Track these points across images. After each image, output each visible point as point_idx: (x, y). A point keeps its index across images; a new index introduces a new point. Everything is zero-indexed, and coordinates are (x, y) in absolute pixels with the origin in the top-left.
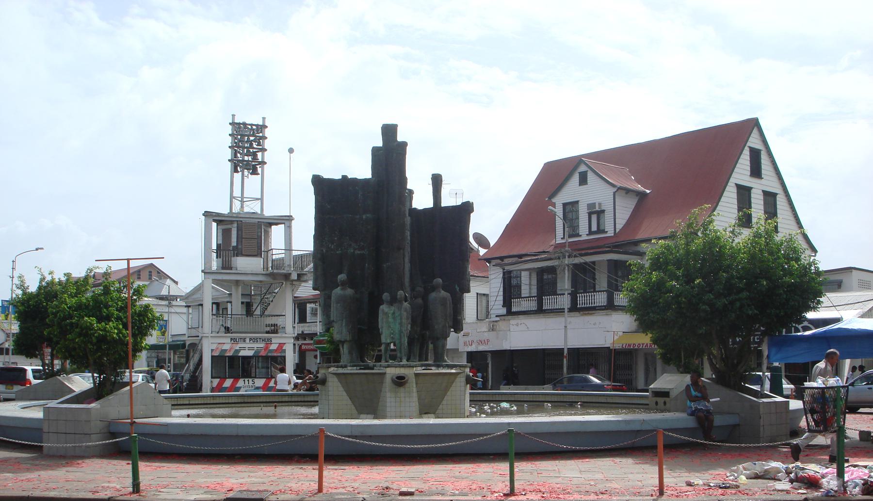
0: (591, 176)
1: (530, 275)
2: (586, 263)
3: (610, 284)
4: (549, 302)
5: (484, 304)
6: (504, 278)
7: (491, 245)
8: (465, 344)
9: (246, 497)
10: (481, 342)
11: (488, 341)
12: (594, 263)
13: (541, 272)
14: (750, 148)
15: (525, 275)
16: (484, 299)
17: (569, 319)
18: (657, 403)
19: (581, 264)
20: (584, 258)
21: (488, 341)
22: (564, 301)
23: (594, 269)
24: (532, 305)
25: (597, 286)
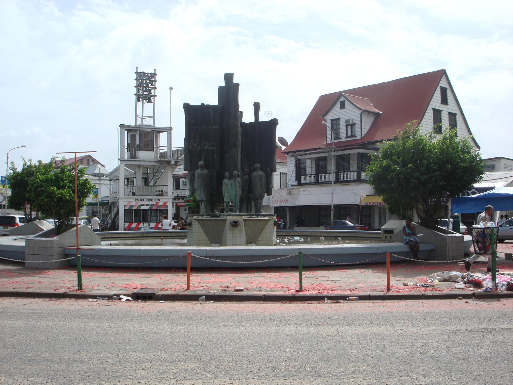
0: (347, 104)
1: (312, 161)
3: (358, 167)
4: (322, 178)
8: (273, 202)
9: (145, 292)
10: (282, 201)
11: (287, 200)
12: (349, 154)
13: (318, 160)
15: (308, 162)
16: (284, 176)
17: (335, 188)
18: (386, 237)
20: (343, 151)
21: (287, 200)
22: (332, 177)
24: (313, 179)
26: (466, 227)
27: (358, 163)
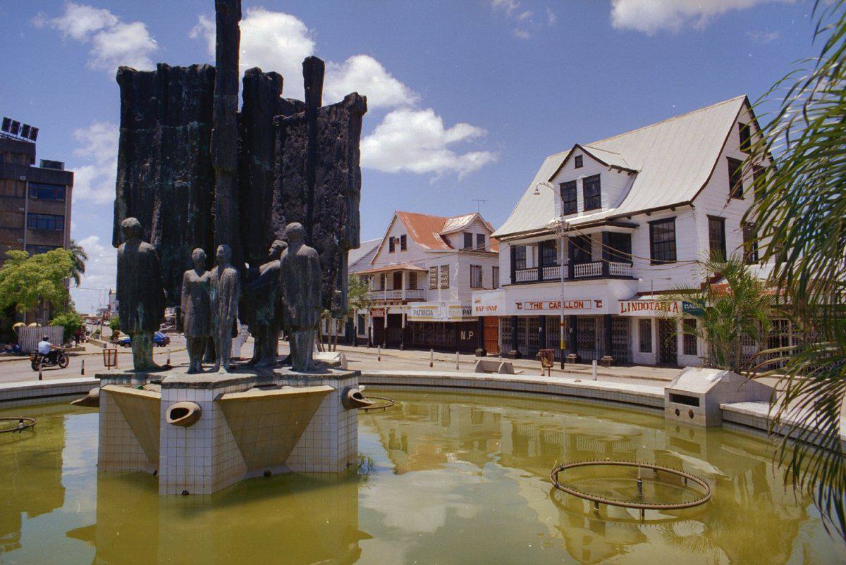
0: (586, 159)
1: (533, 248)
2: (583, 236)
3: (604, 255)
4: (548, 272)
5: (477, 276)
6: (511, 250)
7: (303, 100)
8: (477, 309)
9: (446, 355)
10: (489, 308)
11: (496, 307)
12: (590, 235)
13: (542, 245)
14: (739, 123)
15: (529, 250)
16: (477, 270)
17: (460, 355)
18: (677, 412)
19: (578, 237)
20: (581, 230)
21: (496, 307)
22: (562, 271)
23: (590, 241)
24: (535, 276)
25: (593, 258)
26: (192, 37)
27: (604, 248)
